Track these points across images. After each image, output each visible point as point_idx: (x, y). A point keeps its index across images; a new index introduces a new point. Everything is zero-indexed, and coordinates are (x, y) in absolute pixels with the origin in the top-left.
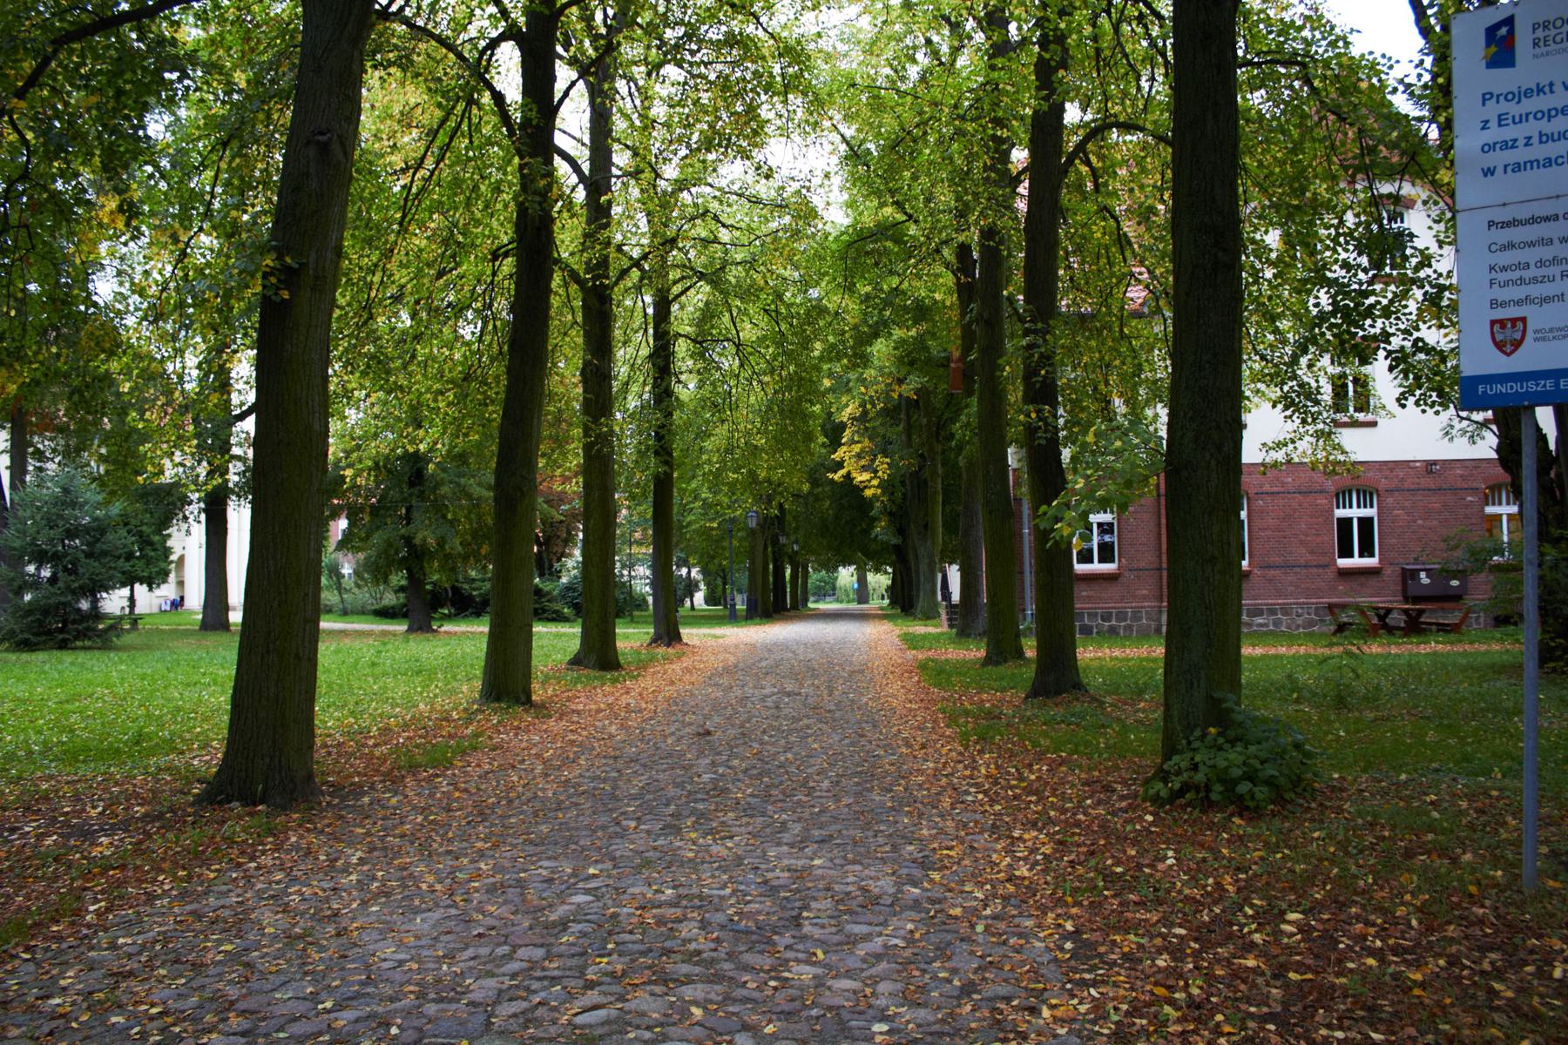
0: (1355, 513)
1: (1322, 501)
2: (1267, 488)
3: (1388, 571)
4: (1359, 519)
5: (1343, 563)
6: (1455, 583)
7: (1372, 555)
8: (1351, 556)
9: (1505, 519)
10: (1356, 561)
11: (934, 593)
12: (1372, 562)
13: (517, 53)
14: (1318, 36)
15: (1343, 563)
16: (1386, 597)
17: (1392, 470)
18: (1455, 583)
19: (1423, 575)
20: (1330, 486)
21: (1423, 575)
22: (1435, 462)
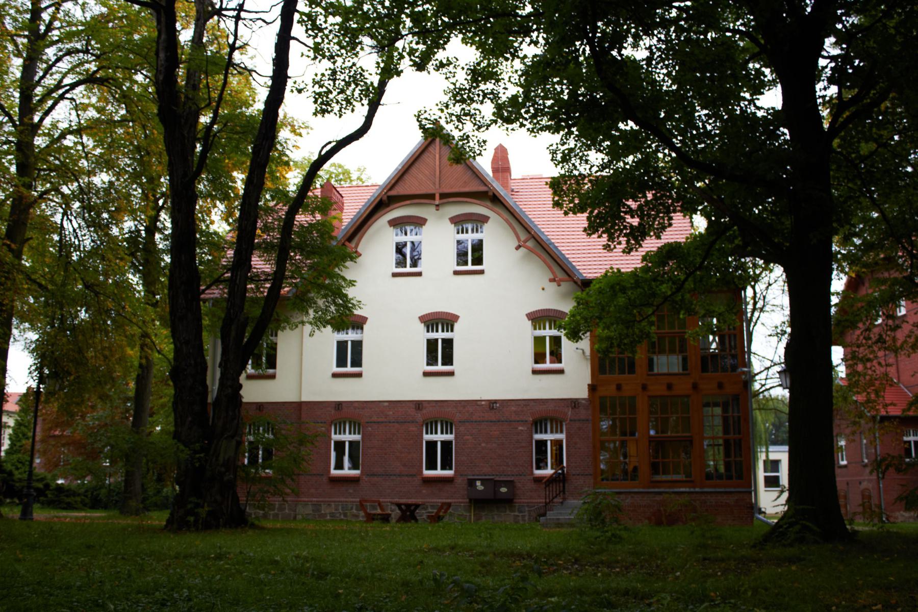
0: (439, 437)
1: (413, 428)
2: (375, 418)
3: (459, 480)
4: (442, 442)
5: (538, 472)
6: (504, 490)
7: (451, 469)
8: (436, 469)
9: (549, 443)
10: (439, 472)
11: (644, 488)
12: (449, 473)
13: (268, 93)
14: (102, 135)
15: (427, 473)
16: (458, 498)
17: (464, 407)
18: (504, 490)
19: (478, 483)
20: (419, 417)
21: (478, 483)
22: (495, 402)
